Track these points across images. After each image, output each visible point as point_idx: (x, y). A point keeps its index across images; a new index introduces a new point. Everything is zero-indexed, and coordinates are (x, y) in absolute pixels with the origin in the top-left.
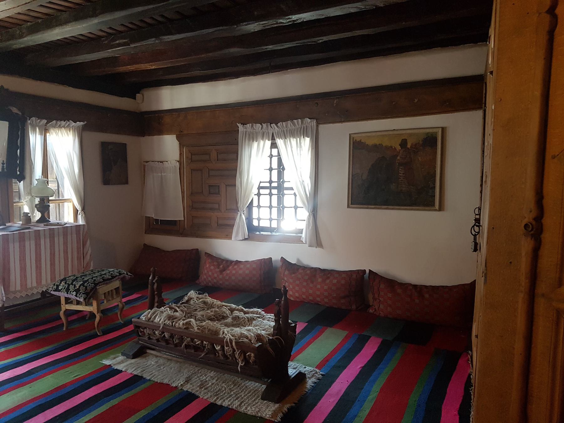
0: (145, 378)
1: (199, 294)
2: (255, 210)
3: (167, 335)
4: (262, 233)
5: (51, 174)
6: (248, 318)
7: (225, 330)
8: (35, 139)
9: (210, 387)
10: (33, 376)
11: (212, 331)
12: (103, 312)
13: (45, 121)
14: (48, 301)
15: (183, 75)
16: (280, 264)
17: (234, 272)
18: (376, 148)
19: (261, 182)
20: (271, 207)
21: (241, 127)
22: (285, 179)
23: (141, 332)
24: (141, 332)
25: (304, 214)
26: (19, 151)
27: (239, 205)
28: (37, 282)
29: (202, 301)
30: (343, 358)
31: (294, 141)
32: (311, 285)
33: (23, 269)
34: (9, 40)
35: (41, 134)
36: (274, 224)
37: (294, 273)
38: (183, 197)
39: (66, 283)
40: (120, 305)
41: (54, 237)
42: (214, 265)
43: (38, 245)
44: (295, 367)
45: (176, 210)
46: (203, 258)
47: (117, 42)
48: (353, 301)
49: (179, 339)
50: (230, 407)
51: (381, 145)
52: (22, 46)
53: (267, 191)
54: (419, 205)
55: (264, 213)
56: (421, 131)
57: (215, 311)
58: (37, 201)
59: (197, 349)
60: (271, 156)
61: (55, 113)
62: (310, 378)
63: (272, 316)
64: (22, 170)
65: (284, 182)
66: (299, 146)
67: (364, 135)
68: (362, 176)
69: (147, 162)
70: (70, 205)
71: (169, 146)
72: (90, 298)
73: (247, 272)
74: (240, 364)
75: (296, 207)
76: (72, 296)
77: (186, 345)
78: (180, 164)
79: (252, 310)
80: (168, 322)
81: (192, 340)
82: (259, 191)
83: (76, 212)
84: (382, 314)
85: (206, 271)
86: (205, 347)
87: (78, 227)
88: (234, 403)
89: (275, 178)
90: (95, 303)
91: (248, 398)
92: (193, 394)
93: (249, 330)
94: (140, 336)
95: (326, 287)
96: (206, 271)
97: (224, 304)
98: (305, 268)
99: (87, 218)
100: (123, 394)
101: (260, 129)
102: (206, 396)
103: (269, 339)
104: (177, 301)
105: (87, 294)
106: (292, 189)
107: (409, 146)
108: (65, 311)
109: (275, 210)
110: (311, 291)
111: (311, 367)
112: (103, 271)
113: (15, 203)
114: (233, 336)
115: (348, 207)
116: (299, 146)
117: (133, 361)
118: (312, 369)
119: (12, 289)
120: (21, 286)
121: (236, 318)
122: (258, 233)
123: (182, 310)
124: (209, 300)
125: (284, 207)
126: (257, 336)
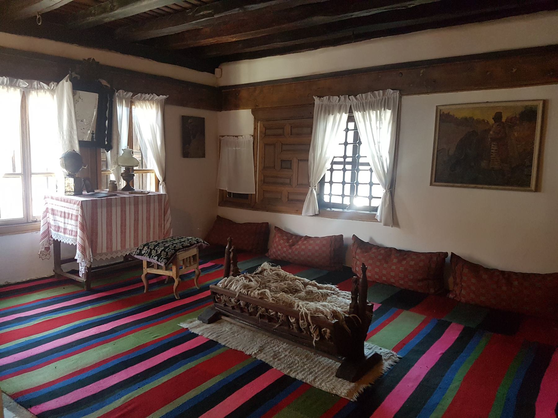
0: (220, 344)
1: (272, 266)
2: (327, 186)
3: (242, 303)
4: (333, 209)
5: (135, 145)
6: (322, 294)
7: (300, 303)
8: (122, 111)
9: (284, 359)
10: (117, 334)
11: (287, 303)
12: (182, 277)
13: (131, 94)
14: (131, 264)
15: (263, 48)
16: (351, 242)
17: (303, 247)
18: (467, 121)
19: (334, 157)
20: (344, 183)
21: (317, 100)
22: (361, 154)
23: (218, 298)
24: (218, 298)
25: (380, 191)
26: (107, 122)
27: (311, 180)
28: (121, 247)
29: (275, 273)
30: (421, 344)
31: (373, 114)
32: (385, 265)
33: (109, 233)
34: (103, 13)
35: (127, 106)
36: (347, 201)
37: (366, 252)
38: (255, 172)
39: (148, 248)
40: (197, 272)
41: (138, 205)
42: (283, 240)
43: (123, 212)
44: (370, 347)
45: (248, 185)
46: (273, 232)
47: (201, 13)
48: (429, 283)
49: (254, 308)
50: (304, 381)
51: (472, 119)
52: (113, 19)
53: (341, 167)
54: (512, 185)
55: (337, 189)
56: (519, 104)
57: (289, 284)
58: (123, 169)
59: (271, 319)
60: (347, 130)
61: (141, 86)
62: (386, 360)
63: (348, 294)
64: (110, 140)
65: (359, 157)
66: (379, 119)
67: (454, 107)
68: (449, 151)
69: (223, 136)
70: (153, 175)
71: (244, 120)
72: (170, 263)
73: (317, 248)
74: (315, 339)
75: (371, 184)
76: (154, 261)
77: (260, 314)
78: (254, 139)
79: (326, 286)
80: (244, 291)
81: (267, 310)
82: (332, 166)
83: (157, 182)
84: (463, 300)
85: (275, 245)
86: (279, 318)
87: (161, 195)
88: (308, 377)
89: (350, 153)
90: (174, 268)
91: (322, 373)
92: (267, 364)
93: (324, 306)
94: (216, 302)
95: (402, 269)
96: (275, 245)
97: (297, 277)
98: (379, 247)
99: (167, 188)
100: (200, 357)
101: (337, 101)
102: (280, 367)
103: (345, 317)
104: (251, 270)
105: (168, 259)
106: (368, 164)
107: (504, 120)
108: (146, 275)
109: (348, 187)
110: (384, 272)
111: (387, 349)
112: (182, 238)
113: (103, 171)
114: (308, 310)
115: (431, 184)
116: (379, 119)
117: (209, 326)
118: (388, 351)
119: (99, 251)
120: (107, 248)
121: (310, 293)
122: (329, 209)
123: (256, 281)
124: (282, 272)
125: (358, 184)
126: (333, 312)
